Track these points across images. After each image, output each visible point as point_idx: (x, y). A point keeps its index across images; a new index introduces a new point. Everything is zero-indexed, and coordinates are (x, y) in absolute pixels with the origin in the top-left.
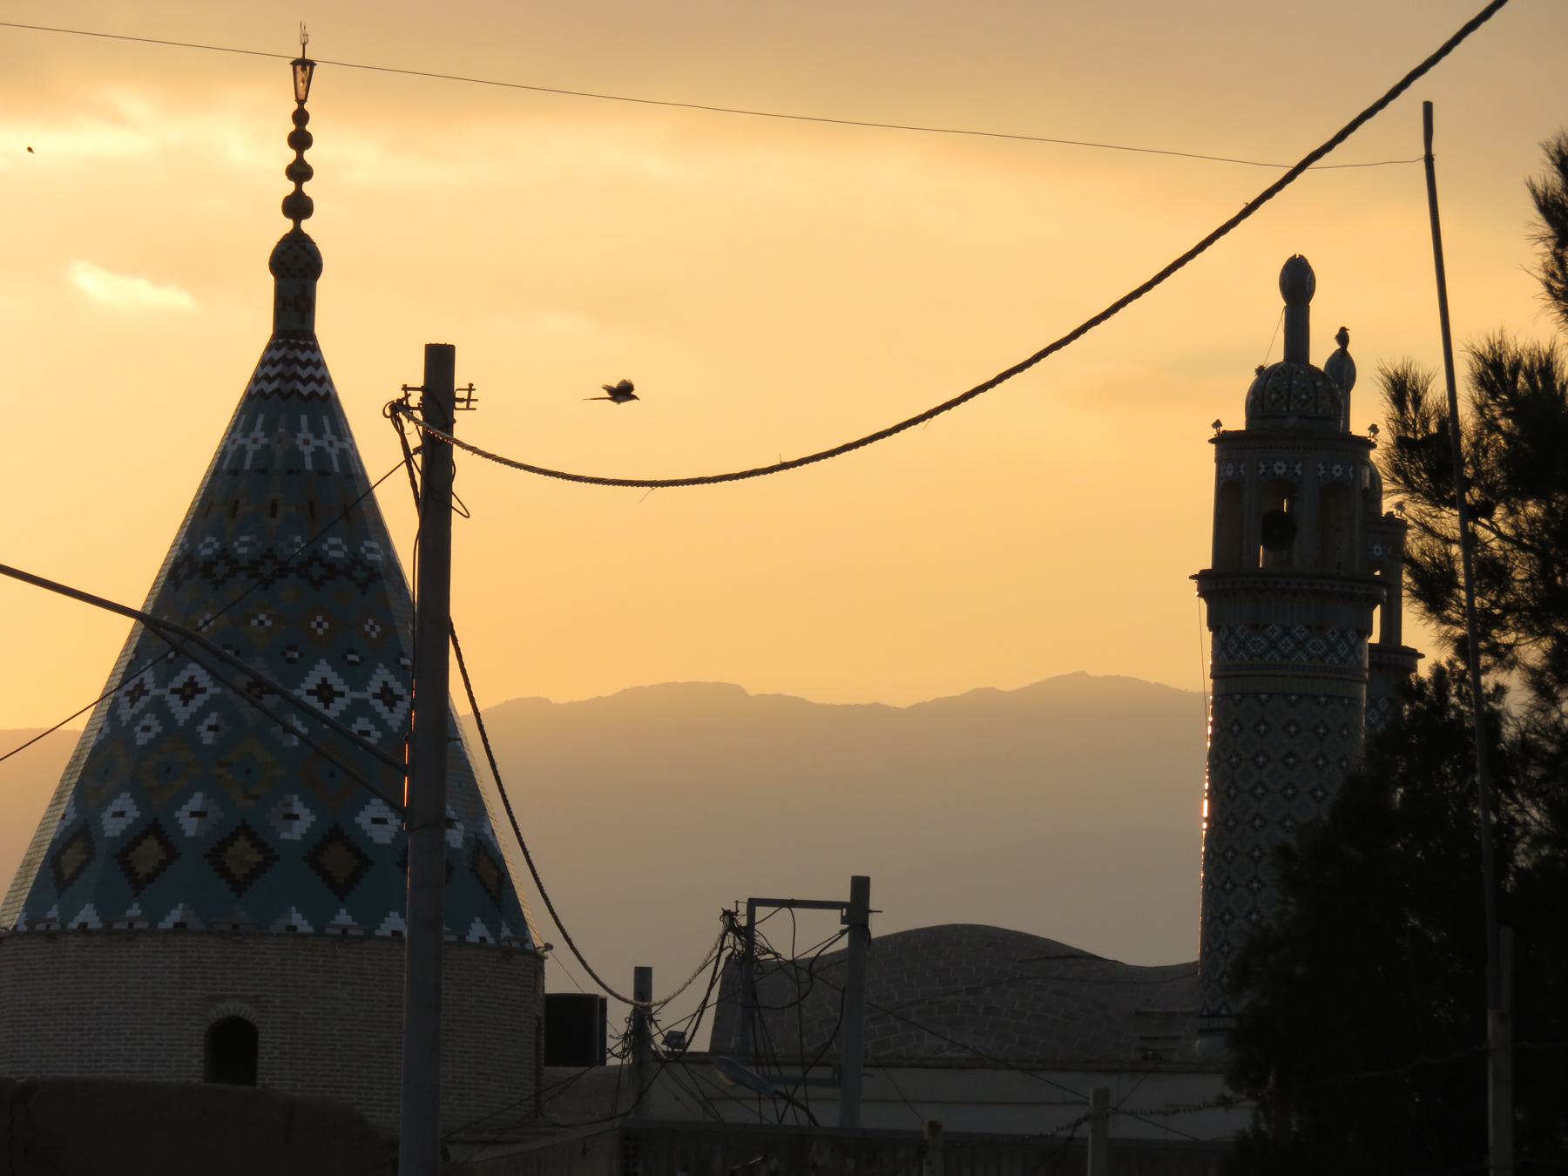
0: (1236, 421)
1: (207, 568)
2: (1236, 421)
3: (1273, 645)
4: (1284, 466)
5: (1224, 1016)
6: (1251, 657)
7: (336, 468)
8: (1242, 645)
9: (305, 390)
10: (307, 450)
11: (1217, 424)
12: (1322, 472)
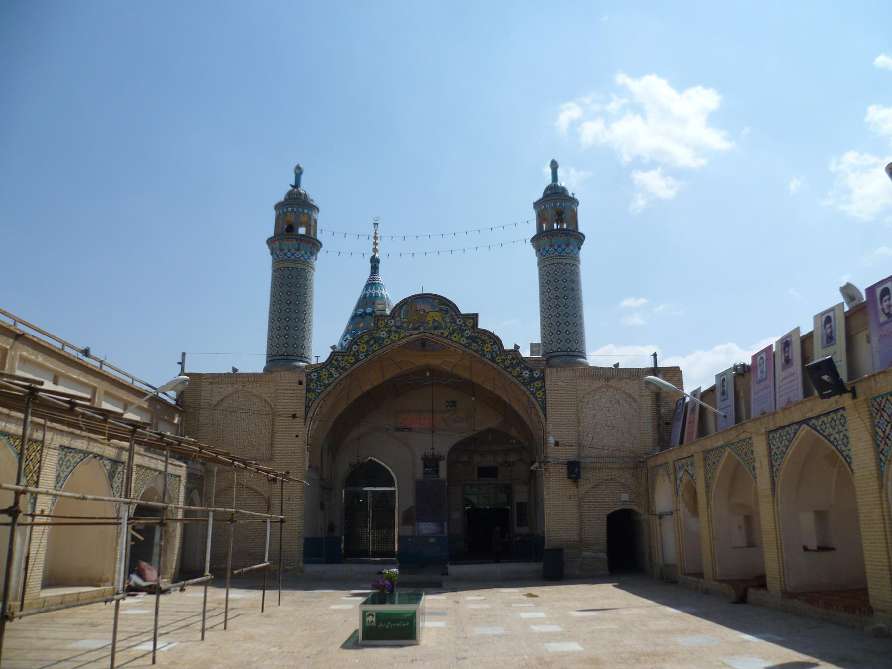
1: (361, 315)
3: (556, 250)
7: (385, 297)
9: (377, 282)
10: (374, 293)
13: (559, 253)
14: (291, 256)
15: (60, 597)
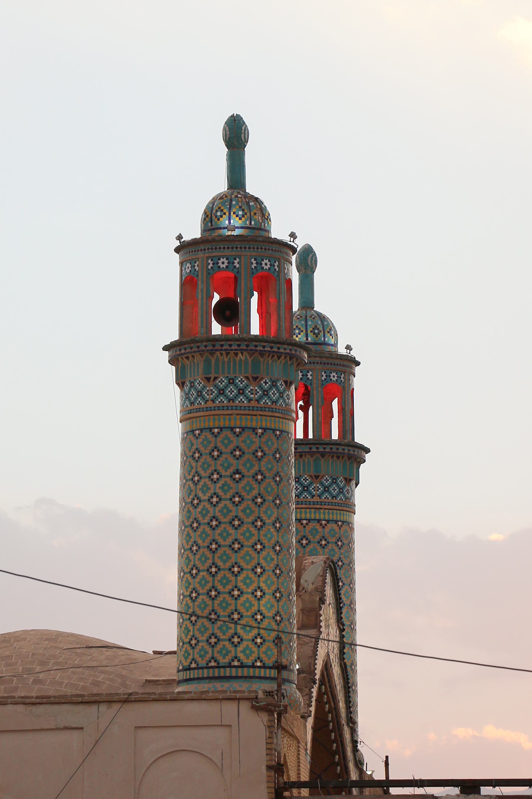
0: (435, 795)
2: (435, 795)
4: (226, 262)
5: (194, 669)
6: (206, 402)
8: (200, 394)
11: (179, 237)
12: (255, 265)
13: (273, 402)
14: (236, 397)
15: (259, 715)
